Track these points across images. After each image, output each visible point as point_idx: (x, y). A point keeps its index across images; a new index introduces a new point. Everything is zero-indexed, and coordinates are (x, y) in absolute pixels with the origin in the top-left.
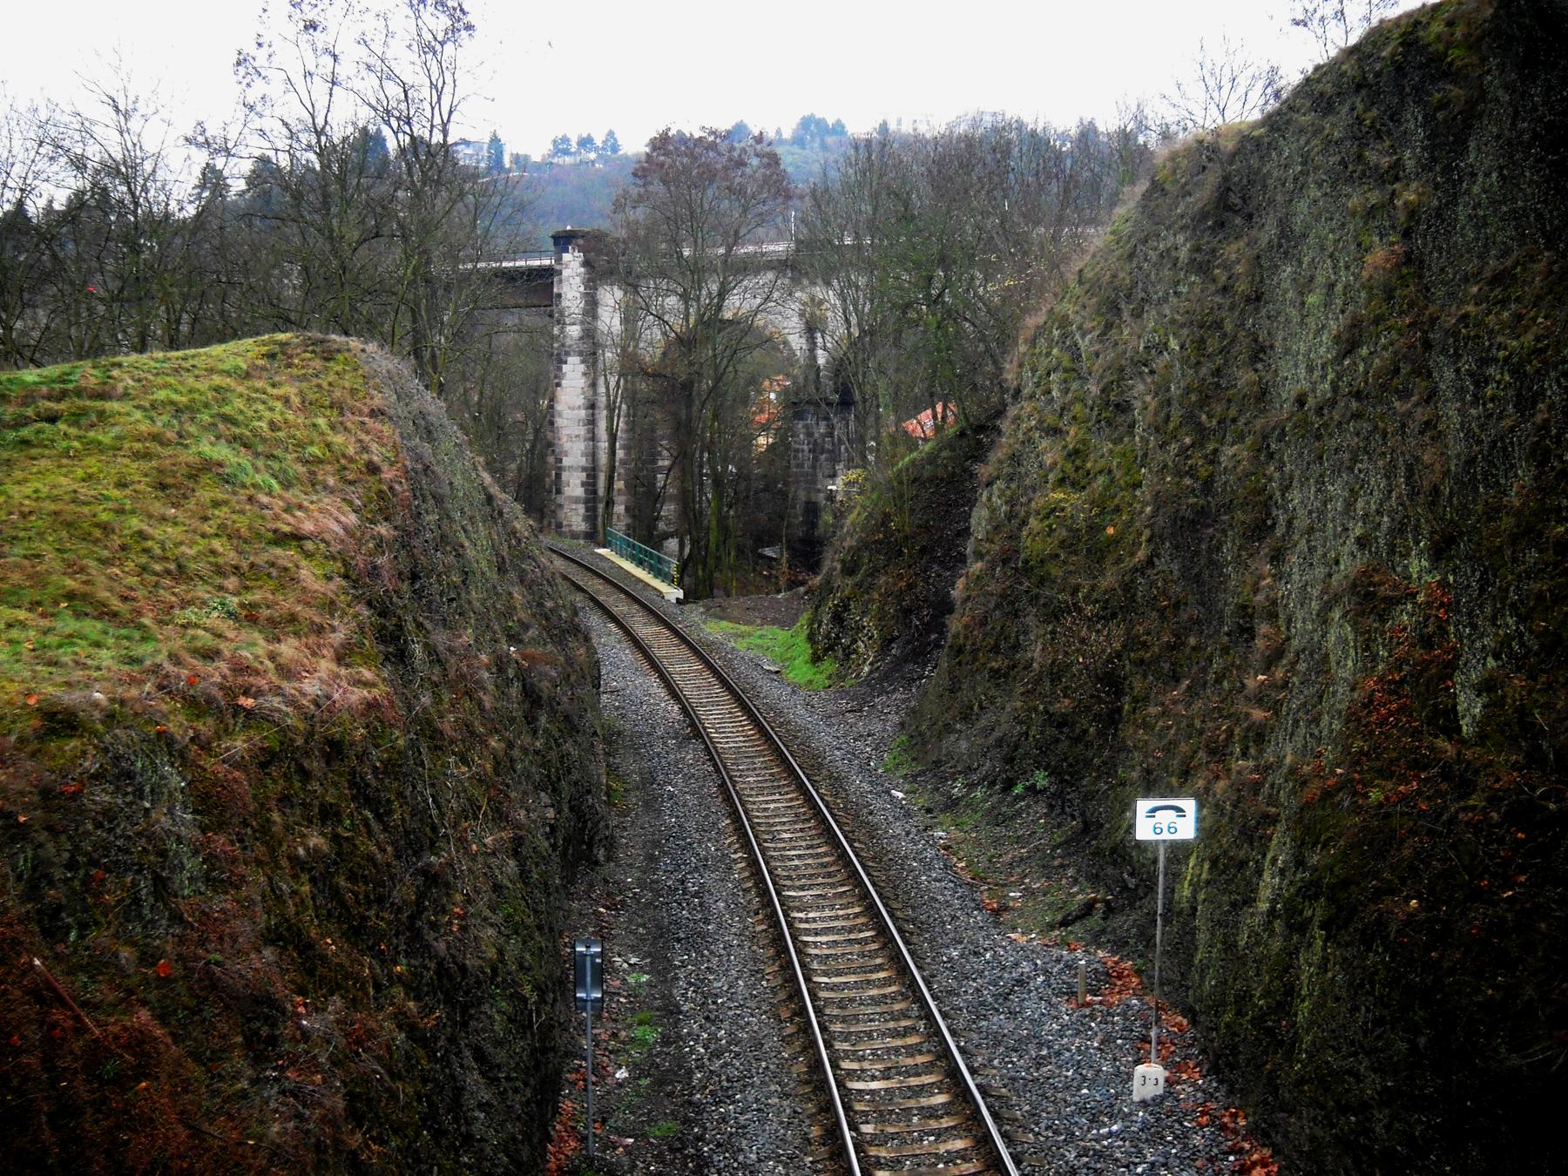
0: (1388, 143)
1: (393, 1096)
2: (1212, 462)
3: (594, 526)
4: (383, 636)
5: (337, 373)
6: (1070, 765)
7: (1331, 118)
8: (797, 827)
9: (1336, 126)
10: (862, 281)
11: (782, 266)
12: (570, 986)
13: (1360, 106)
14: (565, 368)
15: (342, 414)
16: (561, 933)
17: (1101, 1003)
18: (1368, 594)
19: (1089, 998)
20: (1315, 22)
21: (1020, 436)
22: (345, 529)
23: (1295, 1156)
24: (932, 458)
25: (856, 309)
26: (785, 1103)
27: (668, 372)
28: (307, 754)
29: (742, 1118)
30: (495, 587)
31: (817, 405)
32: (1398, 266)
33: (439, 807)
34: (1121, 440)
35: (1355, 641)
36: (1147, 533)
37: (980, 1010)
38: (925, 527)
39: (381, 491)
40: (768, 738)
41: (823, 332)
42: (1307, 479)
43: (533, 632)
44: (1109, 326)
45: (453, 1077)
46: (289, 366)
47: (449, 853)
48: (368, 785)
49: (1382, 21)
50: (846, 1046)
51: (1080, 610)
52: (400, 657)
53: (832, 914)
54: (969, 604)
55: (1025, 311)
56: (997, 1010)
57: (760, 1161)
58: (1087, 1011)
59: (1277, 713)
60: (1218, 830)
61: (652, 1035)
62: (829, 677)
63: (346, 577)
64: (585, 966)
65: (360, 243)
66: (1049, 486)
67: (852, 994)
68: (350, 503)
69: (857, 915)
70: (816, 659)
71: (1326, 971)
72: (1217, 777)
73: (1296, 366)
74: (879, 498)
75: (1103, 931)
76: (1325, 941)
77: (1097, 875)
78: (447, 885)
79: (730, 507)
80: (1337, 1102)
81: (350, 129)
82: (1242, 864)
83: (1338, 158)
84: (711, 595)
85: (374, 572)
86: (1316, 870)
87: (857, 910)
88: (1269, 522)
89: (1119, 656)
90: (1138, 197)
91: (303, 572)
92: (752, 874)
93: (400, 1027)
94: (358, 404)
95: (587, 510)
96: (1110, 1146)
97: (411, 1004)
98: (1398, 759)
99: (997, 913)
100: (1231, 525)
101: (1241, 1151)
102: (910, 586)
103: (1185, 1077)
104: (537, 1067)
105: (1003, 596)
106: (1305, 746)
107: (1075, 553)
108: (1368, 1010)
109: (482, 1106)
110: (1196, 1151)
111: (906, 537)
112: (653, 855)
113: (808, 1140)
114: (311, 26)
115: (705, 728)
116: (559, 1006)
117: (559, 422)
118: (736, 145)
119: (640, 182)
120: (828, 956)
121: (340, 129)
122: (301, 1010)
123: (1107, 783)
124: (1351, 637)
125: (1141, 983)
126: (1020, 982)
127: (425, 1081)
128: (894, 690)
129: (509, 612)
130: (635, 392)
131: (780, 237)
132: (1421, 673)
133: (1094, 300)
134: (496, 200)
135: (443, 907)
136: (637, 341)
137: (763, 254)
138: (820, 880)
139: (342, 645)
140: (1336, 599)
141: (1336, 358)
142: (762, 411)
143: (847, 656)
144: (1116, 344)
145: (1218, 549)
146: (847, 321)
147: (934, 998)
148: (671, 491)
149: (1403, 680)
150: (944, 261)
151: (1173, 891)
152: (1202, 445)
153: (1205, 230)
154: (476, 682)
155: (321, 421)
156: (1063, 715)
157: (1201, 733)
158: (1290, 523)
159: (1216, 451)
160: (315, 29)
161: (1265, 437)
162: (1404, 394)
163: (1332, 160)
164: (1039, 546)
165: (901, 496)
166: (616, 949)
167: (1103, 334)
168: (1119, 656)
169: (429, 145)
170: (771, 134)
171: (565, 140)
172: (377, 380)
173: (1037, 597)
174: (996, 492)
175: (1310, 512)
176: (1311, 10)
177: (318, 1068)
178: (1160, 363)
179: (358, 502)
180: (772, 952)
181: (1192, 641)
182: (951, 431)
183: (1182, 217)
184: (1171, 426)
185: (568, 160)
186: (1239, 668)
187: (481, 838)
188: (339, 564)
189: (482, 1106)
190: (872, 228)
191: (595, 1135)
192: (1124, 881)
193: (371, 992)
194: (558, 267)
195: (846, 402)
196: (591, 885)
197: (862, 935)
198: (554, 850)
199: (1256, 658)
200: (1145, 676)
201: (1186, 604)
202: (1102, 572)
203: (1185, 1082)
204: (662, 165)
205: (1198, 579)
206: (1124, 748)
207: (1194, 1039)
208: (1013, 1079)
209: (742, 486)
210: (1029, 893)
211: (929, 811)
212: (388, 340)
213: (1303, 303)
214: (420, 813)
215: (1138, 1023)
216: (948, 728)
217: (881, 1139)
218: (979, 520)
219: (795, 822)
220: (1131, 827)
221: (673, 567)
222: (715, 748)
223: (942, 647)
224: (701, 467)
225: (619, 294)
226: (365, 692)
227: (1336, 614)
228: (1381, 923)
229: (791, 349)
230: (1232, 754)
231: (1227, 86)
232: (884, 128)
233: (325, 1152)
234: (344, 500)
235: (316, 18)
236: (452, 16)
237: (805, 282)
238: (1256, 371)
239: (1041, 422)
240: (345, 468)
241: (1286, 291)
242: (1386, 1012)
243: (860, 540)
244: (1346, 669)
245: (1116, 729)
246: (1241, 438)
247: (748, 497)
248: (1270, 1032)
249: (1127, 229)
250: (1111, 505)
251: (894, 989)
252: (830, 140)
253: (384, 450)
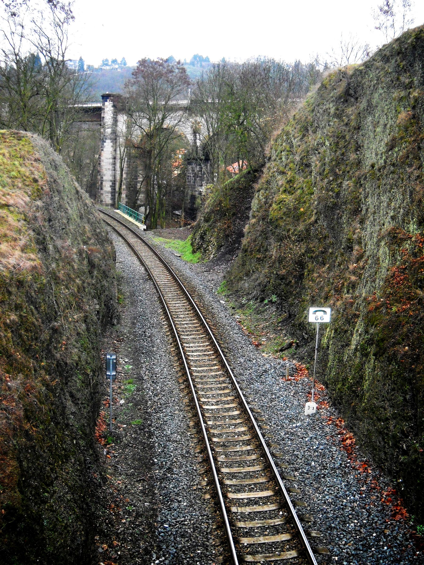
0: (408, 74)
1: (41, 410)
2: (340, 187)
3: (114, 202)
4: (38, 242)
5: (23, 145)
6: (285, 294)
7: (388, 64)
8: (186, 313)
9: (390, 67)
10: (215, 116)
11: (187, 109)
12: (104, 369)
13: (399, 61)
14: (105, 144)
15: (24, 160)
16: (101, 350)
17: (294, 379)
18: (394, 237)
19: (290, 378)
20: (383, 28)
21: (270, 174)
22: (25, 202)
23: (362, 436)
24: (238, 181)
25: (212, 126)
26: (181, 413)
27: (143, 147)
28: (10, 285)
29: (165, 418)
30: (79, 224)
31: (197, 160)
32: (410, 119)
33: (58, 305)
34: (307, 177)
35: (389, 253)
36: (315, 211)
37: (251, 381)
38: (234, 206)
39: (38, 189)
40: (176, 280)
41: (199, 134)
42: (374, 194)
43: (92, 241)
44: (304, 136)
45: (62, 403)
46: (5, 142)
47: (61, 321)
48: (32, 297)
49: (408, 29)
50: (203, 393)
51: (290, 238)
52: (45, 250)
53: (198, 345)
54: (250, 234)
55: (274, 129)
56: (257, 381)
57: (171, 434)
58: (289, 382)
59: (360, 278)
60: (338, 319)
61: (133, 388)
62: (199, 259)
63: (25, 220)
64: (110, 363)
65: (31, 97)
66: (280, 192)
67: (205, 374)
68: (27, 193)
69: (207, 346)
70: (194, 252)
71: (375, 371)
72: (338, 300)
73: (372, 153)
74: (218, 195)
75: (295, 354)
76: (375, 360)
77: (294, 334)
78: (61, 333)
79: (164, 196)
80: (377, 417)
81: (28, 55)
82: (346, 331)
83: (390, 79)
84: (156, 228)
85: (35, 218)
86: (372, 335)
87: (207, 344)
88: (360, 209)
89: (304, 255)
90: (317, 90)
91: (10, 218)
92: (170, 330)
93: (43, 385)
94: (30, 157)
95: (112, 196)
96: (296, 431)
97: (47, 377)
98: (403, 296)
99: (257, 346)
100: (346, 210)
101: (342, 434)
102: (229, 227)
103: (323, 407)
104: (92, 399)
105: (262, 232)
106: (370, 290)
107: (289, 217)
108: (389, 385)
109: (72, 413)
110: (326, 433)
111: (228, 209)
112: (134, 322)
113: (189, 426)
114: (14, 14)
115: (153, 276)
116: (100, 377)
117: (102, 164)
118: (170, 64)
119: (135, 77)
120: (197, 360)
121: (24, 54)
122: (8, 379)
123: (298, 300)
124: (388, 252)
125: (308, 373)
126: (265, 371)
127: (52, 404)
128: (222, 264)
129: (83, 234)
130: (130, 154)
131: (185, 98)
132: (412, 266)
133: (299, 126)
134: (82, 82)
135: (59, 341)
136: (131, 135)
137: (179, 105)
138: (194, 333)
139: (24, 246)
140: (383, 238)
141: (386, 151)
142: (176, 161)
143: (205, 251)
144: (306, 142)
145: (341, 218)
146: (208, 130)
147: (235, 376)
148: (143, 190)
149: (406, 268)
150: (245, 110)
151: (321, 340)
152: (336, 180)
153: (340, 103)
154: (72, 259)
155: (16, 163)
156: (283, 275)
157: (332, 284)
158: (367, 210)
159: (341, 182)
160: (15, 15)
161: (359, 179)
162: (410, 166)
163: (388, 79)
164: (276, 214)
165: (226, 194)
166: (121, 356)
167: (302, 139)
168: (304, 255)
169: (57, 61)
170: (182, 61)
171: (107, 60)
172: (37, 148)
173: (275, 232)
174: (261, 194)
175: (375, 206)
176: (382, 24)
177: (13, 400)
178: (322, 150)
179: (30, 193)
180: (176, 358)
181: (330, 250)
182: (245, 171)
183: (332, 97)
184: (325, 173)
185: (108, 68)
186: (347, 261)
187: (73, 316)
188: (23, 216)
189: (72, 413)
190: (219, 97)
191: (112, 424)
192: (303, 336)
193: (33, 372)
194: (103, 107)
195: (207, 159)
196: (112, 333)
197: (209, 353)
198: (99, 320)
199: (353, 258)
200: (313, 263)
201: (328, 237)
202: (298, 225)
203: (323, 408)
204: (143, 71)
205: (333, 228)
206: (304, 288)
207: (327, 393)
208: (263, 406)
209: (168, 188)
210: (269, 339)
211: (233, 308)
212: (41, 133)
213: (375, 131)
214: (50, 307)
215: (307, 387)
216: (241, 279)
217: (215, 427)
218: (255, 204)
219: (185, 311)
220: (306, 317)
221: (142, 217)
222: (157, 284)
223: (240, 249)
224: (154, 181)
225: (125, 118)
226: (32, 263)
227: (383, 243)
228: (395, 355)
229: (187, 139)
230: (343, 292)
231: (350, 50)
232: (223, 60)
233: (17, 431)
234: (25, 192)
235: (16, 11)
236: (66, 13)
237: (193, 115)
238: (357, 154)
239: (278, 169)
240: (25, 180)
241: (369, 126)
242: (395, 386)
243: (211, 209)
244: (385, 263)
245: (302, 281)
246: (350, 178)
247: (170, 193)
248: (354, 392)
249: (312, 101)
250: (302, 200)
251: (220, 372)
252: (203, 64)
253: (39, 174)
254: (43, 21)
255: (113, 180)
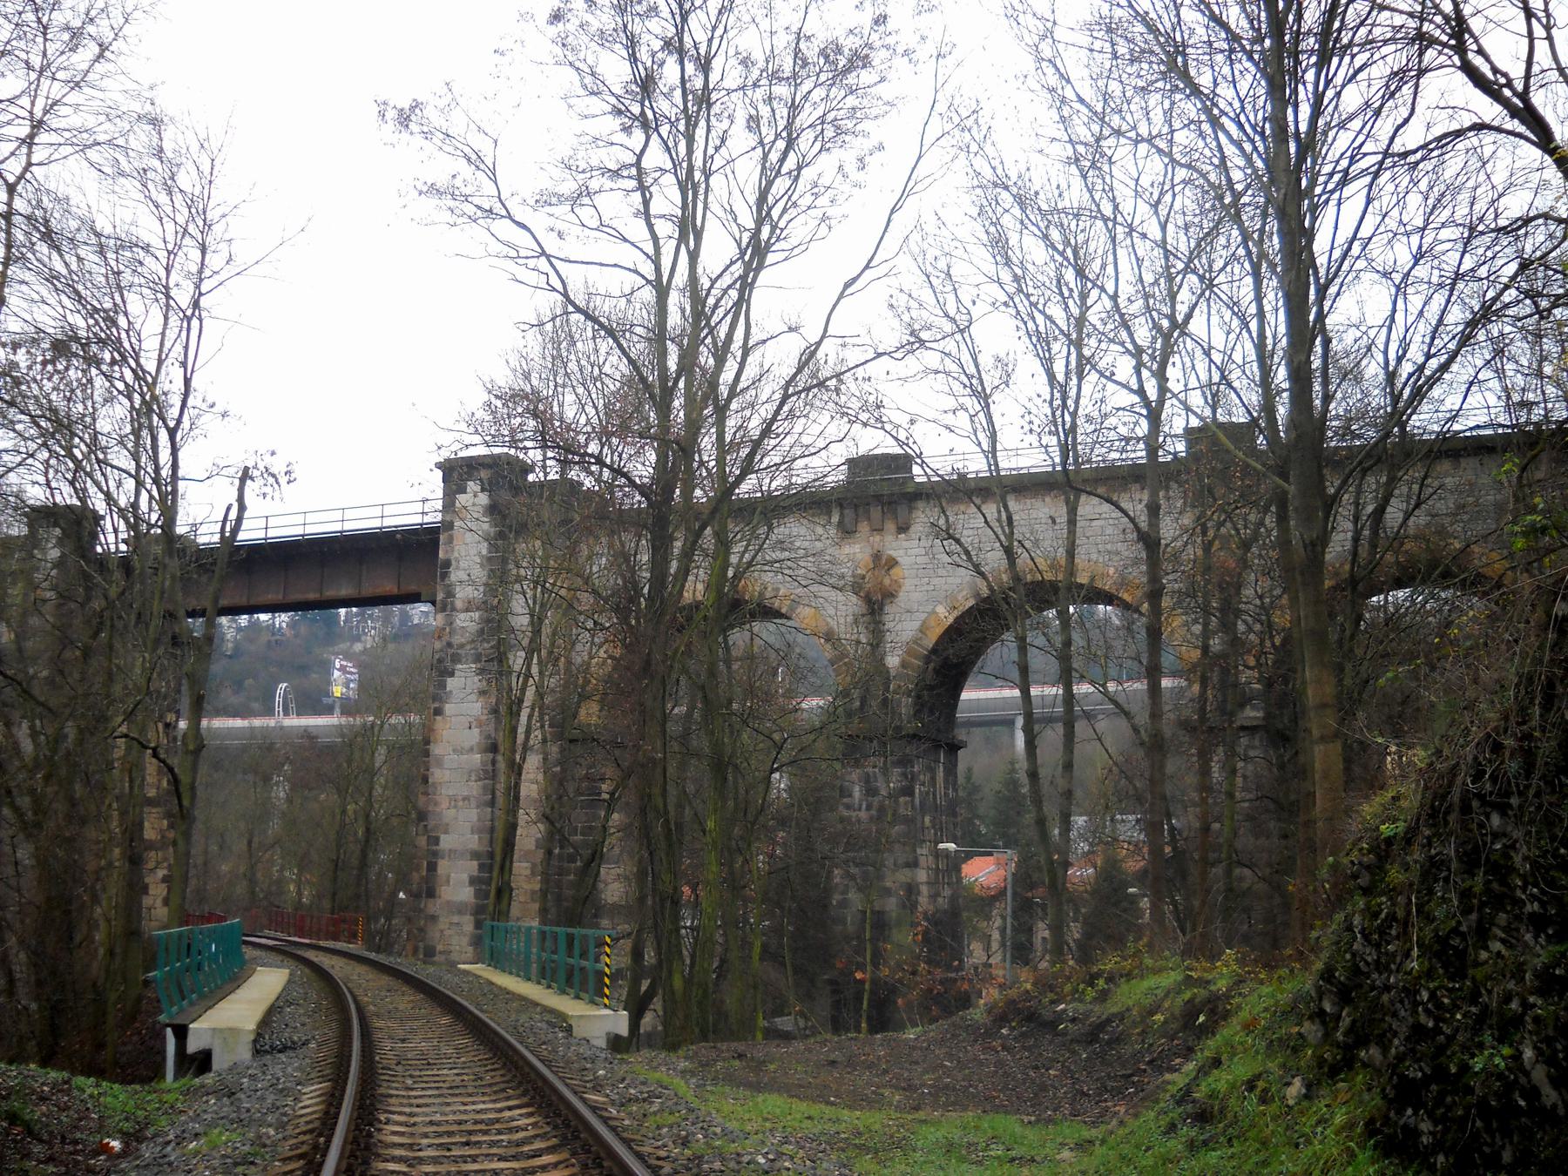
117: (437, 775)
131: (817, 691)
254: (218, 409)
255: (486, 848)
